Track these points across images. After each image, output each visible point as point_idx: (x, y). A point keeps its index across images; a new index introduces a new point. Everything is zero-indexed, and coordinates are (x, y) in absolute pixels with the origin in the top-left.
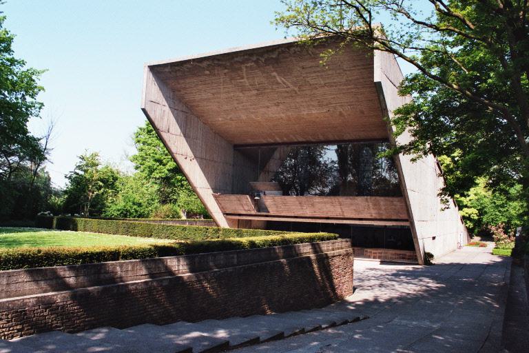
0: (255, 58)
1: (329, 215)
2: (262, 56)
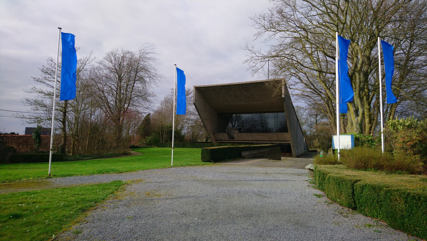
0: (238, 87)
1: (259, 140)
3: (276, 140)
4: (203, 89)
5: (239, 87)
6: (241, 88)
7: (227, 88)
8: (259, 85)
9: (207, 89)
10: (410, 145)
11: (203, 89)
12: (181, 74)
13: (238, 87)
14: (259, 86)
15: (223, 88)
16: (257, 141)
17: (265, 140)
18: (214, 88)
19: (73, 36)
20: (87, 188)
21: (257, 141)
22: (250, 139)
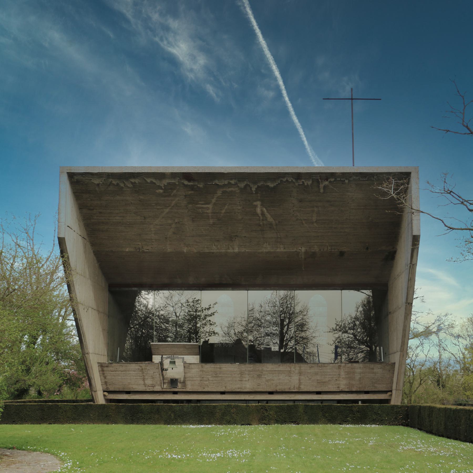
0: (242, 185)
1: (279, 388)
2: (255, 183)
3: (343, 387)
4: (96, 181)
5: (247, 185)
6: (254, 189)
7: (201, 186)
8: (326, 183)
9: (114, 182)
10: (256, 346)
11: (96, 181)
12: (213, 314)
13: (242, 185)
14: (325, 187)
15: (186, 183)
16: (271, 393)
17: (304, 389)
18: (149, 180)
19: (64, 238)
20: (30, 421)
21: (271, 393)
22: (248, 386)
